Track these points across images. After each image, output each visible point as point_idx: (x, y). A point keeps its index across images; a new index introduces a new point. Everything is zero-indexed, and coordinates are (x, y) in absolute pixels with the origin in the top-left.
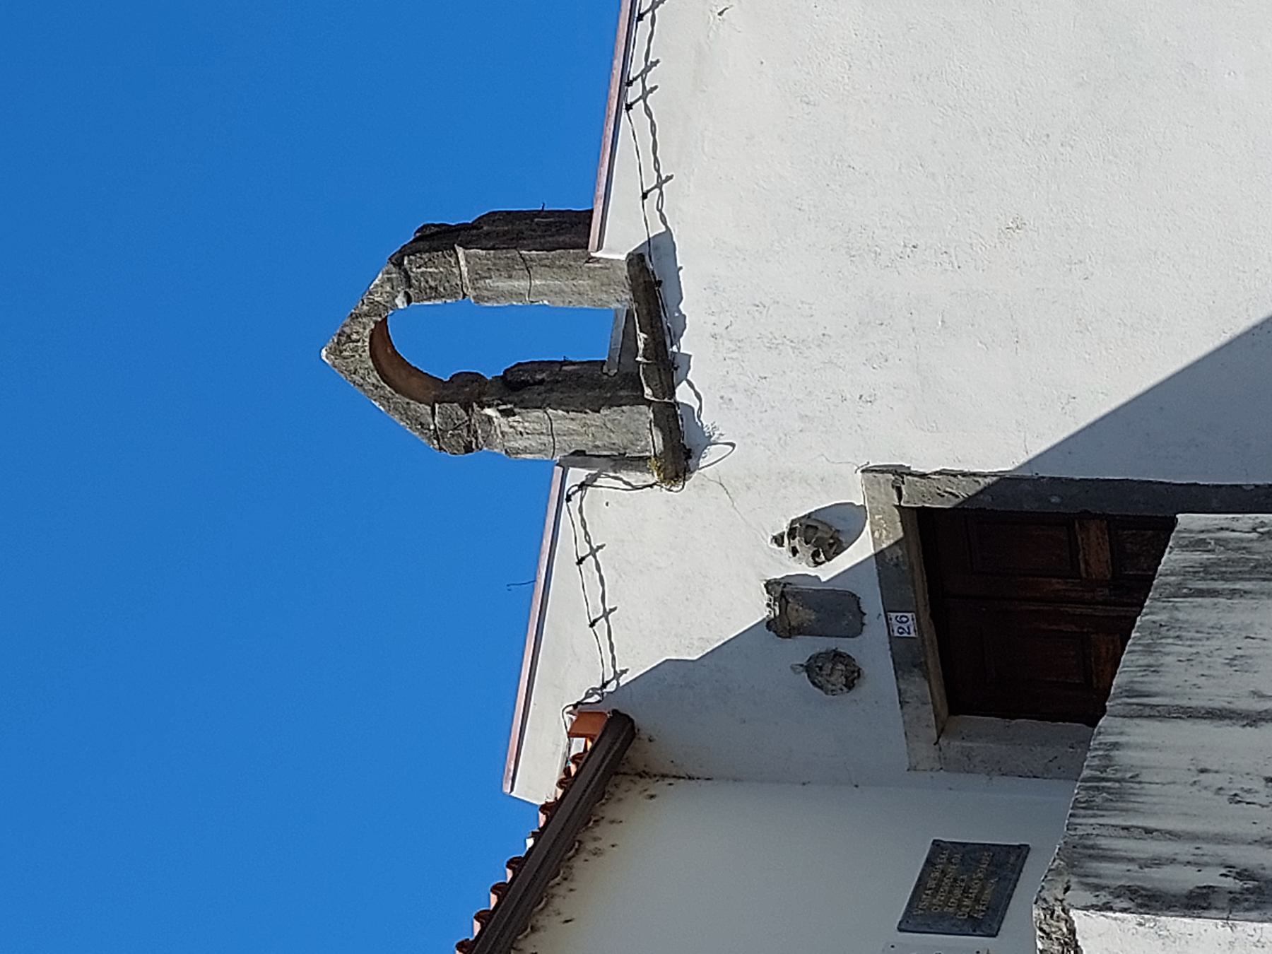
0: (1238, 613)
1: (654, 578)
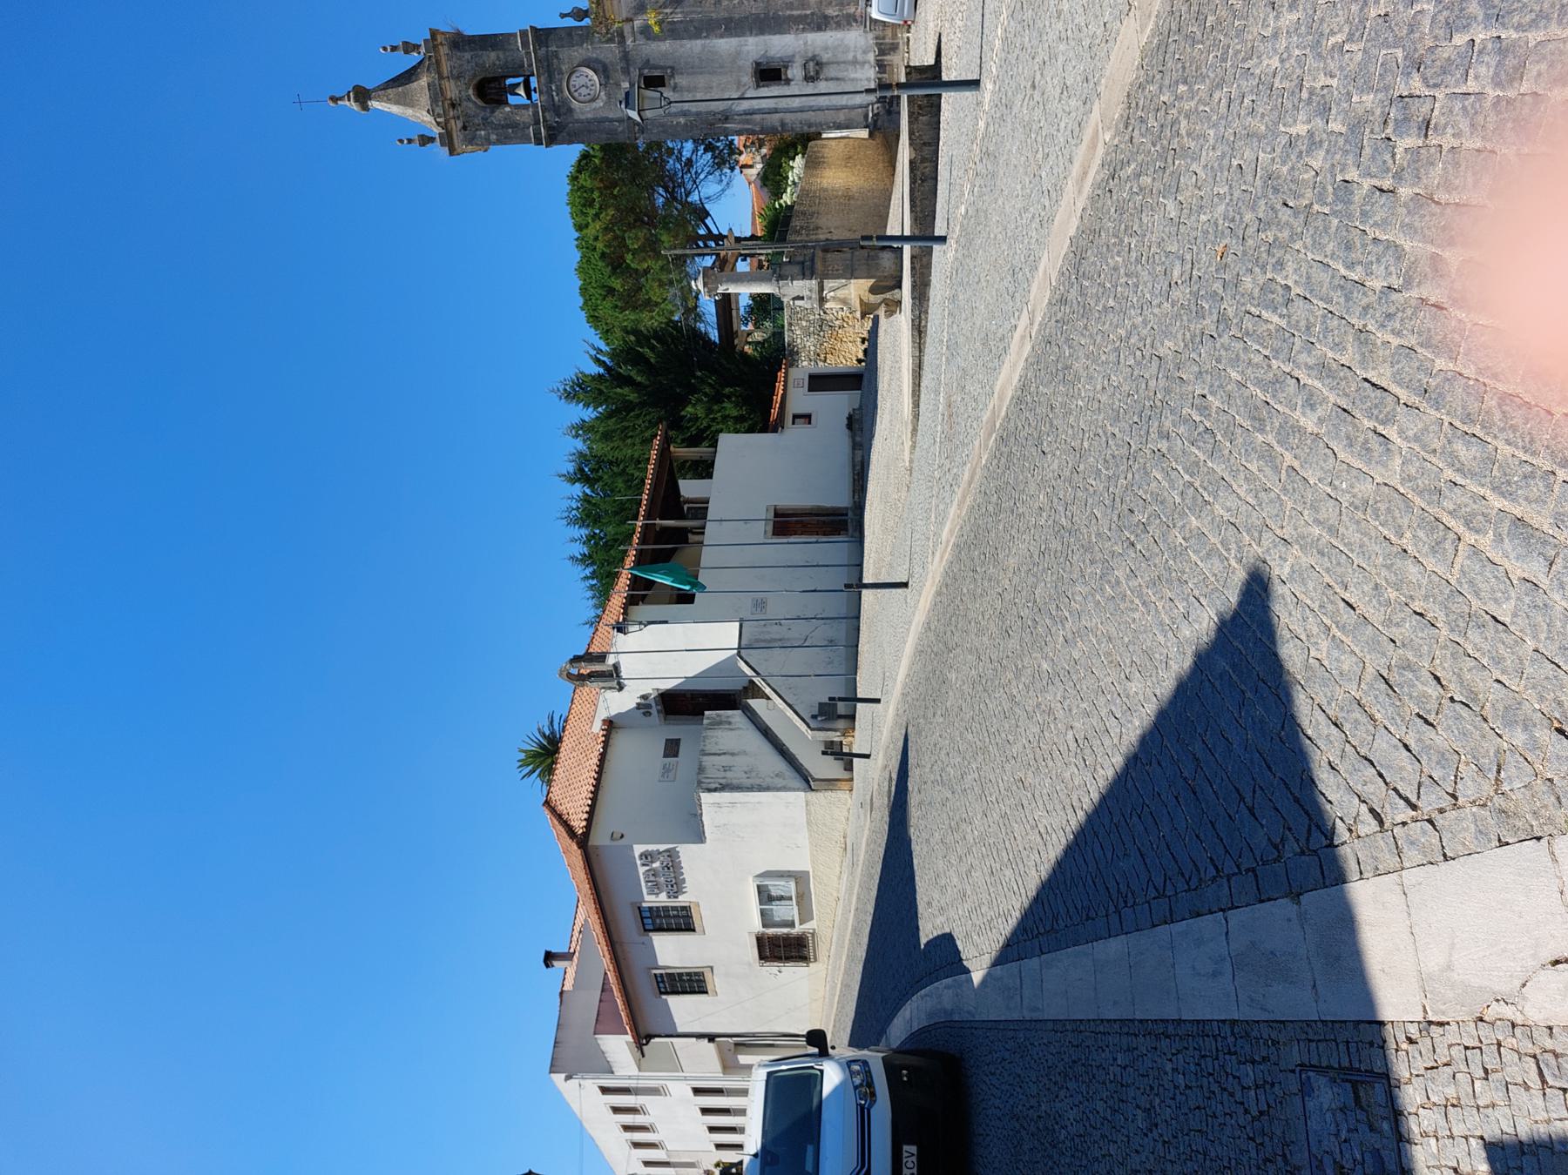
0: (719, 733)
1: (618, 703)
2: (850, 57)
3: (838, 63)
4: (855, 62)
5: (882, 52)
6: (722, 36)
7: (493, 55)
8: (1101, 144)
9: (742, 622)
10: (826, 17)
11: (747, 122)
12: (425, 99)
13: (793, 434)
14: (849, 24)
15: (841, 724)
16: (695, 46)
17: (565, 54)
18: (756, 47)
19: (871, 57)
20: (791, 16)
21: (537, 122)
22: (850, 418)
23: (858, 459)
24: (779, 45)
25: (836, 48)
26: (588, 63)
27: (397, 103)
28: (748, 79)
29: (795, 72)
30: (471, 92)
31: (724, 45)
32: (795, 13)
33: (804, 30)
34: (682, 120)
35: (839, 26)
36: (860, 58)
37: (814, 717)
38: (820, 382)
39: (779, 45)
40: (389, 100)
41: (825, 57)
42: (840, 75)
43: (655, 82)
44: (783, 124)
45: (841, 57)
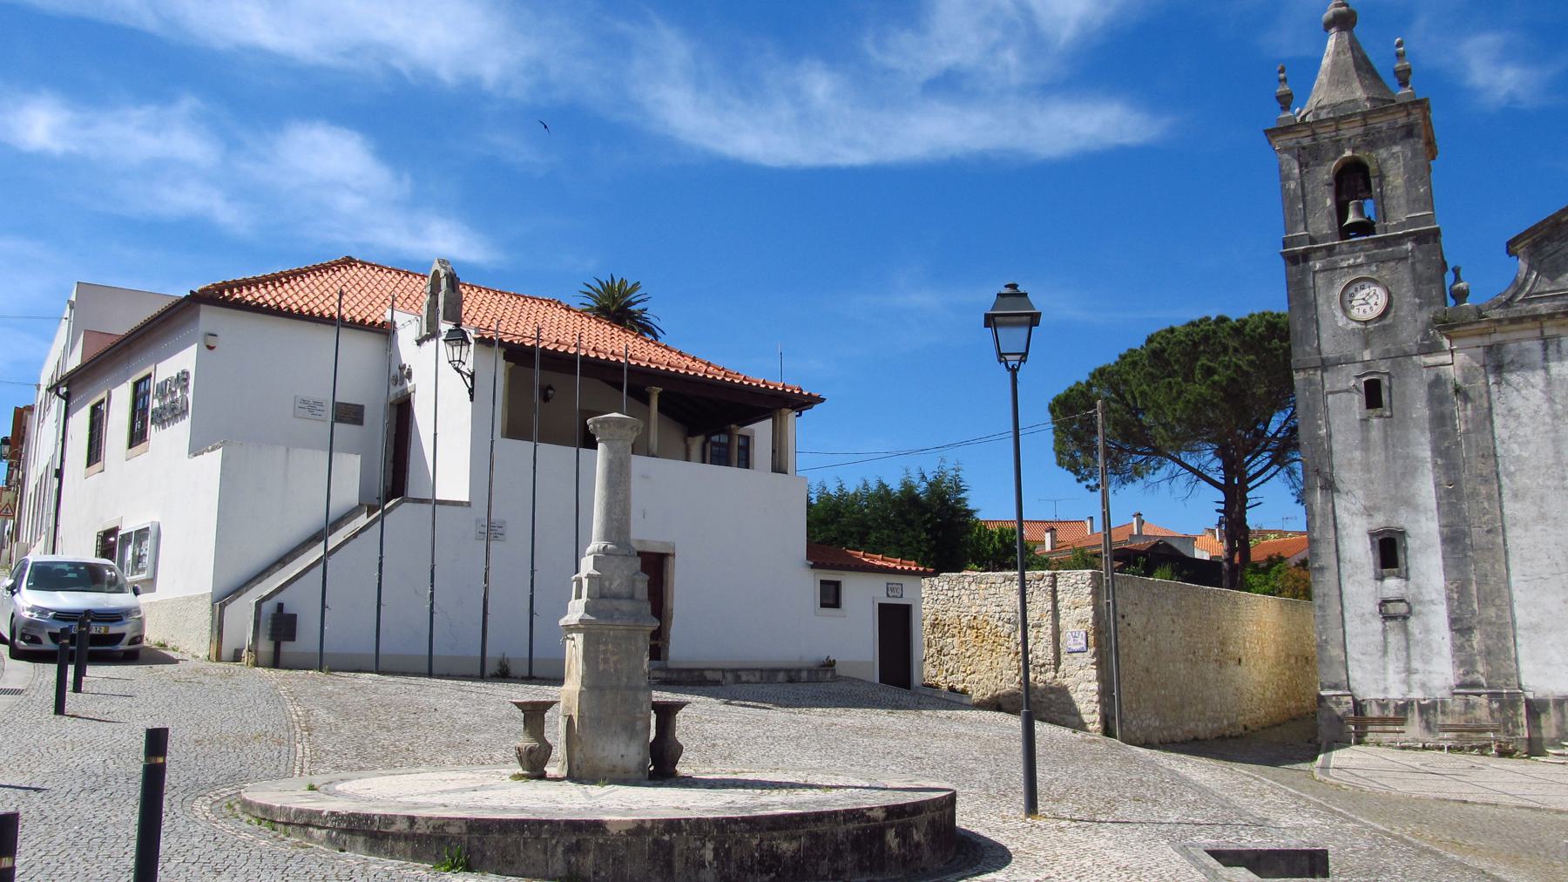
2: (1416, 664)
3: (1408, 648)
4: (1409, 671)
5: (1424, 710)
6: (1437, 485)
7: (1399, 181)
8: (66, 625)
9: (469, 504)
10: (1470, 630)
11: (1324, 515)
12: (1339, 96)
13: (809, 583)
14: (1462, 663)
15: (266, 646)
16: (1423, 448)
17: (1403, 272)
18: (1425, 536)
19: (1417, 694)
20: (1469, 581)
21: (1312, 240)
22: (829, 665)
23: (709, 675)
24: (1428, 566)
25: (1429, 645)
26: (1345, 311)
27: (1334, 64)
28: (1379, 521)
29: (1392, 586)
30: (1348, 153)
31: (1426, 488)
32: (1474, 588)
33: (1449, 599)
34: (1323, 432)
35: (1458, 649)
36: (1416, 678)
37: (280, 606)
38: (896, 624)
39: (1428, 566)
40: (1337, 53)
41: (1413, 624)
42: (1391, 650)
43: (1373, 394)
44: (1321, 569)
45: (1414, 652)
